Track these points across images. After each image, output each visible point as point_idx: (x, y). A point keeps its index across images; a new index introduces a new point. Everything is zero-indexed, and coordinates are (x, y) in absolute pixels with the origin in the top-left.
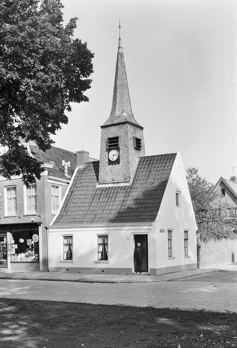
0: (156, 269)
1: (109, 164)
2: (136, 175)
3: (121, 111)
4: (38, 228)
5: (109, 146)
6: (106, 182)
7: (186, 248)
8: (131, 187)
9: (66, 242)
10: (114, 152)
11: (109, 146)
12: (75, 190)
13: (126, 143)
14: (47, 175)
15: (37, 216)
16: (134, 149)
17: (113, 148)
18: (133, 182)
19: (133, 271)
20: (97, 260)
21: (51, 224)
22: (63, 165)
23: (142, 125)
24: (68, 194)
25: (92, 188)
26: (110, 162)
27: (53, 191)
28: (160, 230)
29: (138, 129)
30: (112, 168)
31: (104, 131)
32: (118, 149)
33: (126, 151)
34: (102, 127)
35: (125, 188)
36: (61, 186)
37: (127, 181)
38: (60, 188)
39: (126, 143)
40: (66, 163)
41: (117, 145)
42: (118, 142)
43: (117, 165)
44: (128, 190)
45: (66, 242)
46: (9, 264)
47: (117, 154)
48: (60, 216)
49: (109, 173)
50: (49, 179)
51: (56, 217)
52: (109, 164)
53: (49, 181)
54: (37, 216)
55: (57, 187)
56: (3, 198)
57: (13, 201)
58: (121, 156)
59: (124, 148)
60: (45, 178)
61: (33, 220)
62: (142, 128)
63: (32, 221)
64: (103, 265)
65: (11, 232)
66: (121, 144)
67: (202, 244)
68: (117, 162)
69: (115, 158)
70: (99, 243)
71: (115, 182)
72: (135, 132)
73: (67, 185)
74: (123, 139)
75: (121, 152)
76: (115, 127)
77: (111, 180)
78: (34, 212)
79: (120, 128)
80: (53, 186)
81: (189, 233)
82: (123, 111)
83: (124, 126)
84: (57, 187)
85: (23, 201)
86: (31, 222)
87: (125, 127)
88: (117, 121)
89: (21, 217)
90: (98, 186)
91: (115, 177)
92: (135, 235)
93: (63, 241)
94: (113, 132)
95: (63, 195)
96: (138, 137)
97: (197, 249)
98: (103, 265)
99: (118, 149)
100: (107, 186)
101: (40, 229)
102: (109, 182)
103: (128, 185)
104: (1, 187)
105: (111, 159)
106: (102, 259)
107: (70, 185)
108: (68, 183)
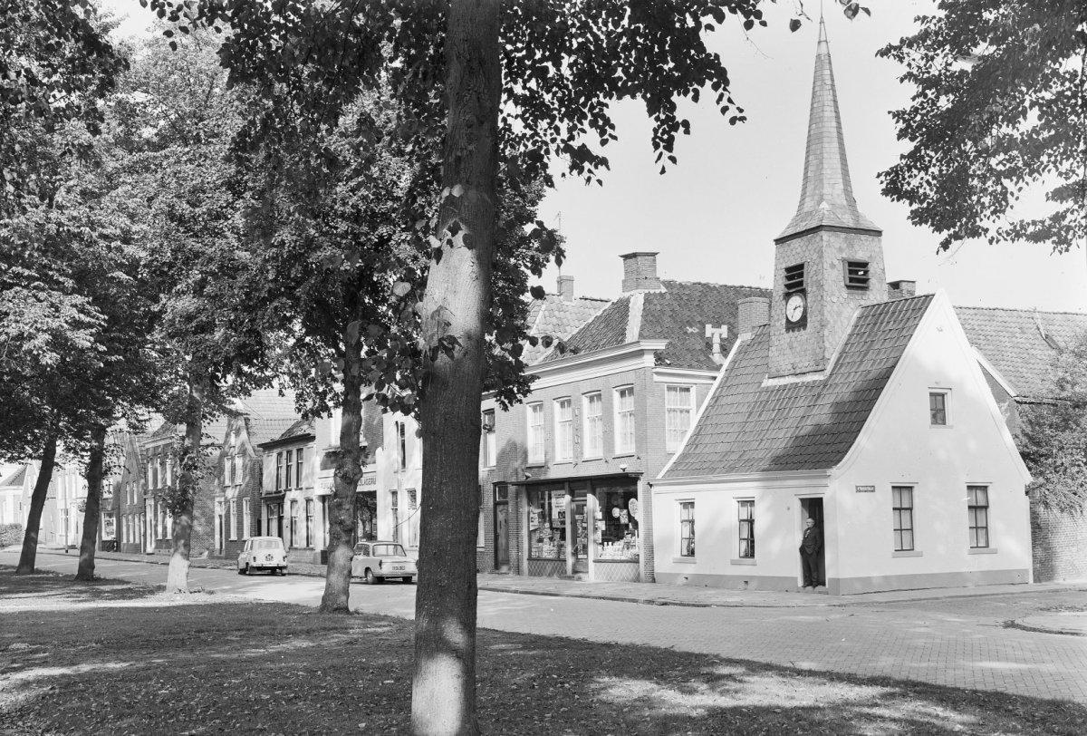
0: (839, 579)
1: (788, 330)
2: (843, 352)
3: (816, 198)
4: (636, 484)
5: (787, 286)
6: (782, 373)
7: (982, 533)
8: (825, 384)
9: (685, 515)
10: (796, 301)
11: (787, 286)
12: (723, 394)
13: (820, 277)
14: (653, 365)
15: (635, 458)
16: (845, 289)
17: (794, 290)
18: (834, 369)
19: (800, 583)
20: (737, 557)
21: (659, 477)
22: (708, 334)
23: (878, 226)
24: (709, 403)
25: (752, 389)
26: (791, 326)
27: (672, 400)
28: (857, 487)
29: (863, 237)
30: (793, 339)
31: (781, 250)
32: (803, 292)
33: (819, 298)
34: (779, 241)
35: (810, 386)
36: (694, 386)
37: (820, 368)
38: (693, 390)
39: (820, 277)
40: (714, 330)
41: (801, 283)
42: (801, 275)
43: (802, 332)
44: (817, 391)
45: (685, 515)
46: (591, 565)
47: (802, 304)
48: (684, 456)
49: (788, 351)
50: (658, 373)
51: (674, 459)
52: (788, 330)
53: (656, 378)
54: (635, 458)
55: (688, 390)
56: (581, 420)
57: (631, 422)
58: (809, 310)
59: (815, 289)
60: (648, 373)
61: (623, 466)
62: (879, 233)
63: (624, 470)
64: (746, 569)
65: (594, 494)
66: (808, 279)
67: (1051, 516)
68: (802, 323)
69: (796, 316)
70: (741, 518)
71: (798, 372)
72: (851, 245)
73: (711, 382)
74: (814, 268)
75: (809, 300)
76: (799, 240)
77: (790, 367)
78: (632, 451)
79: (809, 241)
80: (669, 389)
81: (915, 492)
82: (821, 200)
83: (816, 237)
84: (688, 390)
85: (612, 424)
86: (621, 471)
87: (818, 239)
88: (804, 224)
89: (610, 460)
90: (768, 383)
91: (797, 360)
92: (807, 499)
93: (679, 513)
94: (793, 257)
95: (699, 406)
96: (860, 256)
97: (1032, 532)
98: (746, 569)
99: (803, 292)
100: (782, 382)
101: (641, 486)
102: (786, 373)
103: (822, 378)
104: (577, 394)
105: (790, 318)
106: (746, 556)
107: (716, 383)
108: (715, 378)
